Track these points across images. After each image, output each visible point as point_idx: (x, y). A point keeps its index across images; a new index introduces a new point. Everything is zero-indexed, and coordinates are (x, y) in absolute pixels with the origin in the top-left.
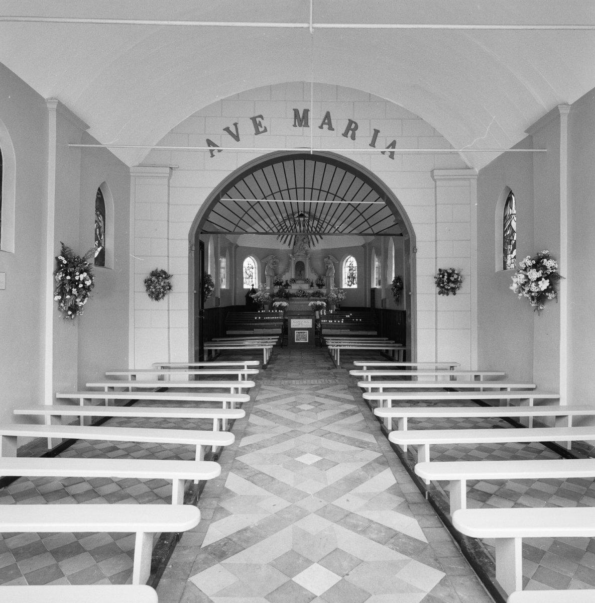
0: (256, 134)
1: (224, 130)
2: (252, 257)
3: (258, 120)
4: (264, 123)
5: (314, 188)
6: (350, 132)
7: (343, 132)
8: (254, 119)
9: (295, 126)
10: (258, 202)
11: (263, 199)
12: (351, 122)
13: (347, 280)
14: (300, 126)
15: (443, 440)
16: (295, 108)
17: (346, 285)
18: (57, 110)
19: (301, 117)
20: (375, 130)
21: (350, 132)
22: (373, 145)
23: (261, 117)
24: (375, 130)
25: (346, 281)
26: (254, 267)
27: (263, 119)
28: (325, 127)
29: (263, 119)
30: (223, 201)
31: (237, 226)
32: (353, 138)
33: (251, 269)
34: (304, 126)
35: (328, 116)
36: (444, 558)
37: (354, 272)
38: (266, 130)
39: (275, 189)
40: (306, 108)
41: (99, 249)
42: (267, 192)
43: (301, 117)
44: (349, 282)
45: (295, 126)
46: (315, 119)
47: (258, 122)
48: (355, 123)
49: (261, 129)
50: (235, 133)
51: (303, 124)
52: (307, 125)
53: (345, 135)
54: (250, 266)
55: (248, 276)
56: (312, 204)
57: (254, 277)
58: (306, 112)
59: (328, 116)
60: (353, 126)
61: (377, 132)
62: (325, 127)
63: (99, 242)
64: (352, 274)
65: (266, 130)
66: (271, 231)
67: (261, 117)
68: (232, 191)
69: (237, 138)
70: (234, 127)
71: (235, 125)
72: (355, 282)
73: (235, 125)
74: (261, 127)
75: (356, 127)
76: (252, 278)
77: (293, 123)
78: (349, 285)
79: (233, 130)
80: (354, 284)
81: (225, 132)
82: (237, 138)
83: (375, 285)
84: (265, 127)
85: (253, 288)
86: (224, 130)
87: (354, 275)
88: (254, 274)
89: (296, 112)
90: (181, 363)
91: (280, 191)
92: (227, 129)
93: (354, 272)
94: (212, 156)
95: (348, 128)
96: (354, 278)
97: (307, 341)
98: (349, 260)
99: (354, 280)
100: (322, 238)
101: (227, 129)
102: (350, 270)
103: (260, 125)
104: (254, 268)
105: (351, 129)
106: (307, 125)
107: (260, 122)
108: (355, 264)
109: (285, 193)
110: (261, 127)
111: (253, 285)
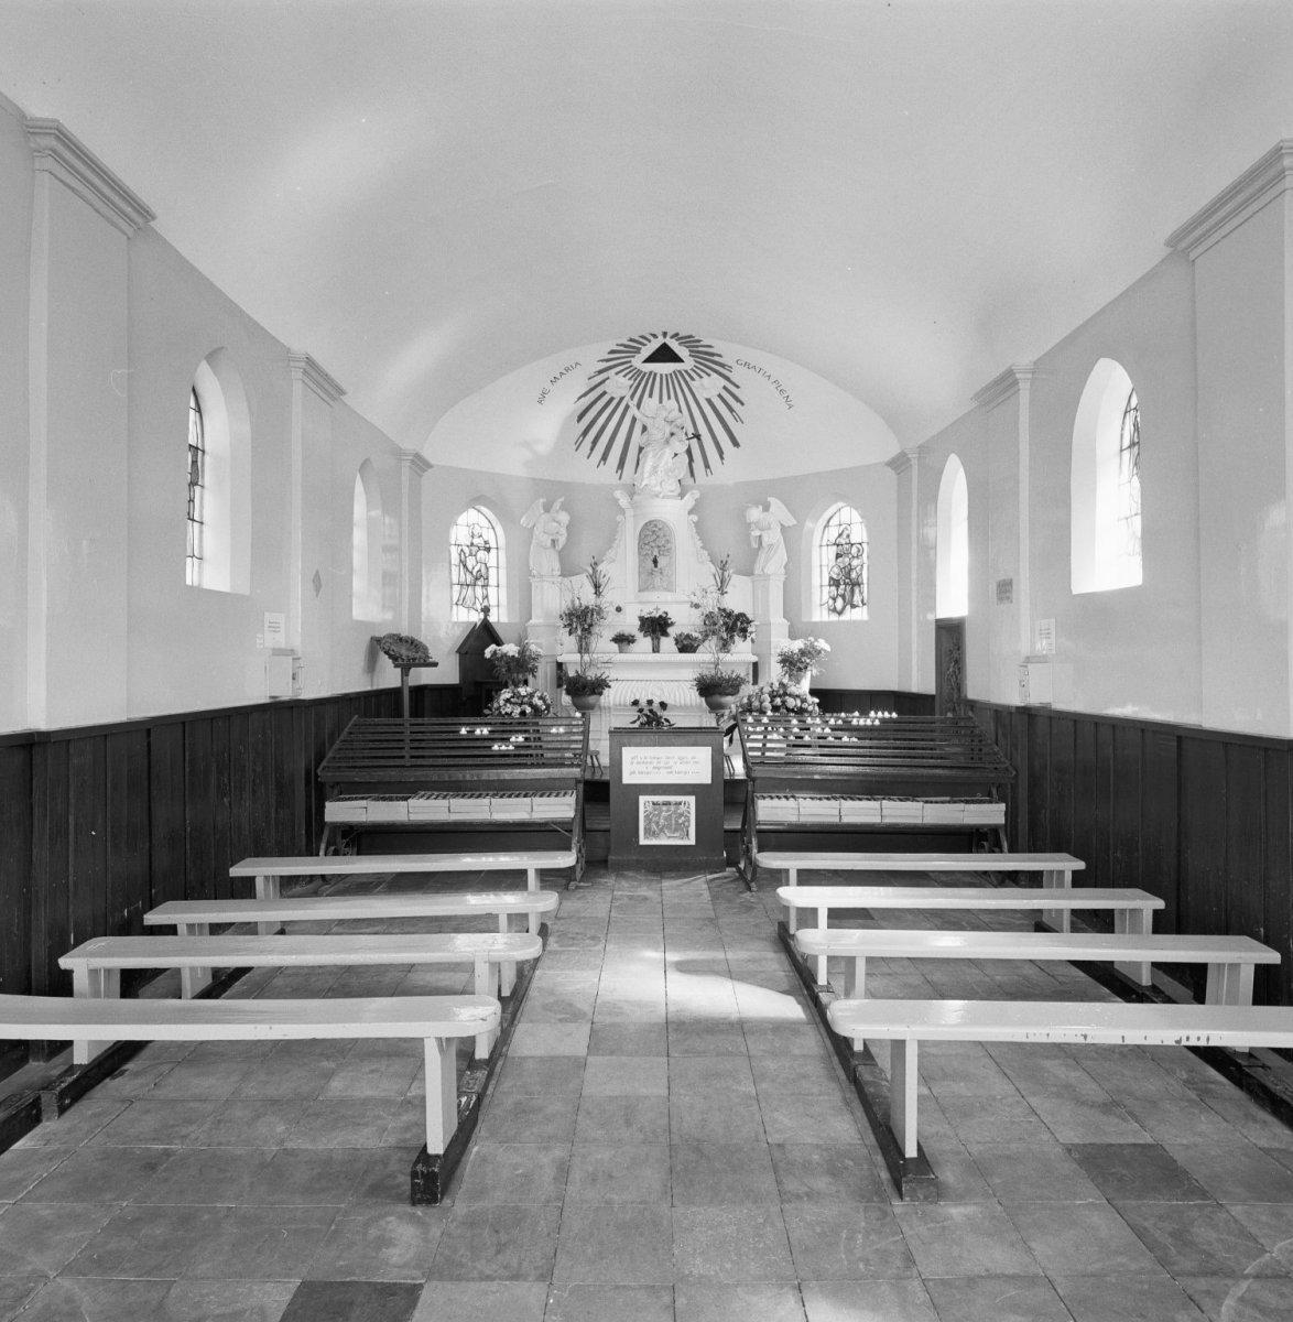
2: (483, 509)
13: (828, 591)
17: (825, 612)
25: (826, 597)
26: (493, 544)
33: (482, 554)
37: (855, 562)
44: (834, 599)
54: (476, 541)
55: (469, 579)
64: (848, 570)
72: (857, 599)
76: (485, 586)
78: (834, 610)
80: (853, 606)
83: (953, 602)
87: (854, 575)
88: (492, 573)
90: (942, 802)
93: (855, 562)
97: (643, 841)
98: (834, 521)
99: (852, 592)
100: (736, 443)
102: (838, 556)
108: (859, 534)
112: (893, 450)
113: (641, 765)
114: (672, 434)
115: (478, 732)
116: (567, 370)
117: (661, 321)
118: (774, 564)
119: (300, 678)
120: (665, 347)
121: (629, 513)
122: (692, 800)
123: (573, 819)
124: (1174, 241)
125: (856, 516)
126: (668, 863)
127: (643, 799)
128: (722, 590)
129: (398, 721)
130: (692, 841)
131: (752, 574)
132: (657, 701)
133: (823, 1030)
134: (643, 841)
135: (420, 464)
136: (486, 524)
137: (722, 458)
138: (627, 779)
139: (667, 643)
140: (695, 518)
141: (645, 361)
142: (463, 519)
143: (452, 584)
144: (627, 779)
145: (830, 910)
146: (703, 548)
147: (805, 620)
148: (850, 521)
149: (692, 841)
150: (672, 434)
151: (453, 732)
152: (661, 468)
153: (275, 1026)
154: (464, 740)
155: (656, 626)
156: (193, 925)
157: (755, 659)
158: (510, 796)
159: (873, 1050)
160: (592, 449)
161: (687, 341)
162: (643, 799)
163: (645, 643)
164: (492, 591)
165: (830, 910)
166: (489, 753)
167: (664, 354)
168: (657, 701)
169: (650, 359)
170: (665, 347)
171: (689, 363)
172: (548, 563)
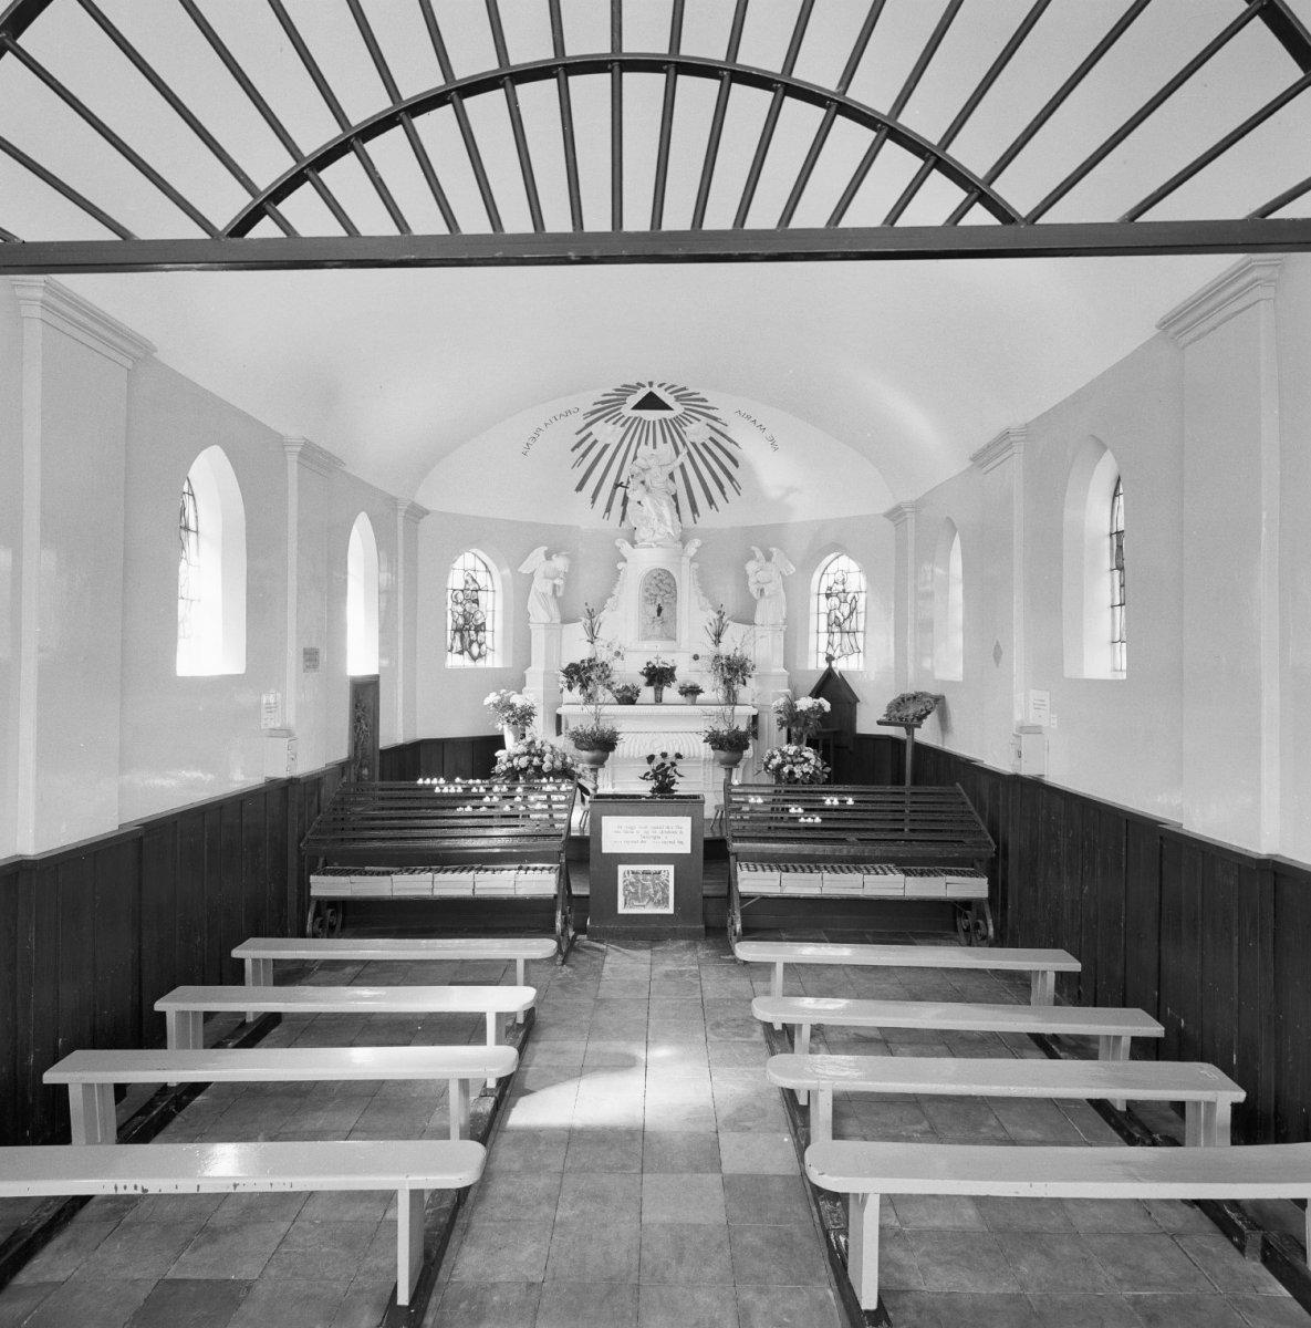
26: (823, 598)
88: (823, 627)
96: (459, 630)
97: (621, 910)
108: (856, 581)
112: (888, 505)
113: (619, 835)
114: (643, 482)
115: (836, 802)
116: (749, 417)
117: (654, 372)
118: (768, 612)
119: (1013, 751)
120: (651, 395)
122: (671, 868)
123: (556, 897)
124: (1165, 324)
125: (853, 566)
126: (645, 932)
127: (622, 869)
128: (717, 642)
129: (900, 789)
130: (670, 910)
131: (751, 622)
132: (671, 754)
133: (499, 1114)
134: (621, 910)
135: (417, 513)
136: (483, 568)
137: (593, 502)
138: (606, 849)
139: (671, 693)
140: (696, 565)
141: (633, 408)
142: (459, 564)
143: (864, 632)
144: (606, 849)
145: (785, 964)
146: (612, 596)
147: (800, 668)
148: (844, 570)
149: (670, 910)
150: (643, 482)
151: (817, 801)
152: (654, 515)
153: (1050, 1184)
154: (850, 810)
155: (659, 676)
156: (91, 1085)
157: (755, 712)
158: (454, 871)
159: (1136, 1111)
160: (724, 493)
161: (683, 395)
162: (622, 869)
163: (648, 693)
164: (823, 647)
165: (785, 964)
166: (795, 825)
167: (651, 402)
168: (671, 754)
169: (638, 407)
170: (651, 395)
171: (678, 409)
172: (541, 613)
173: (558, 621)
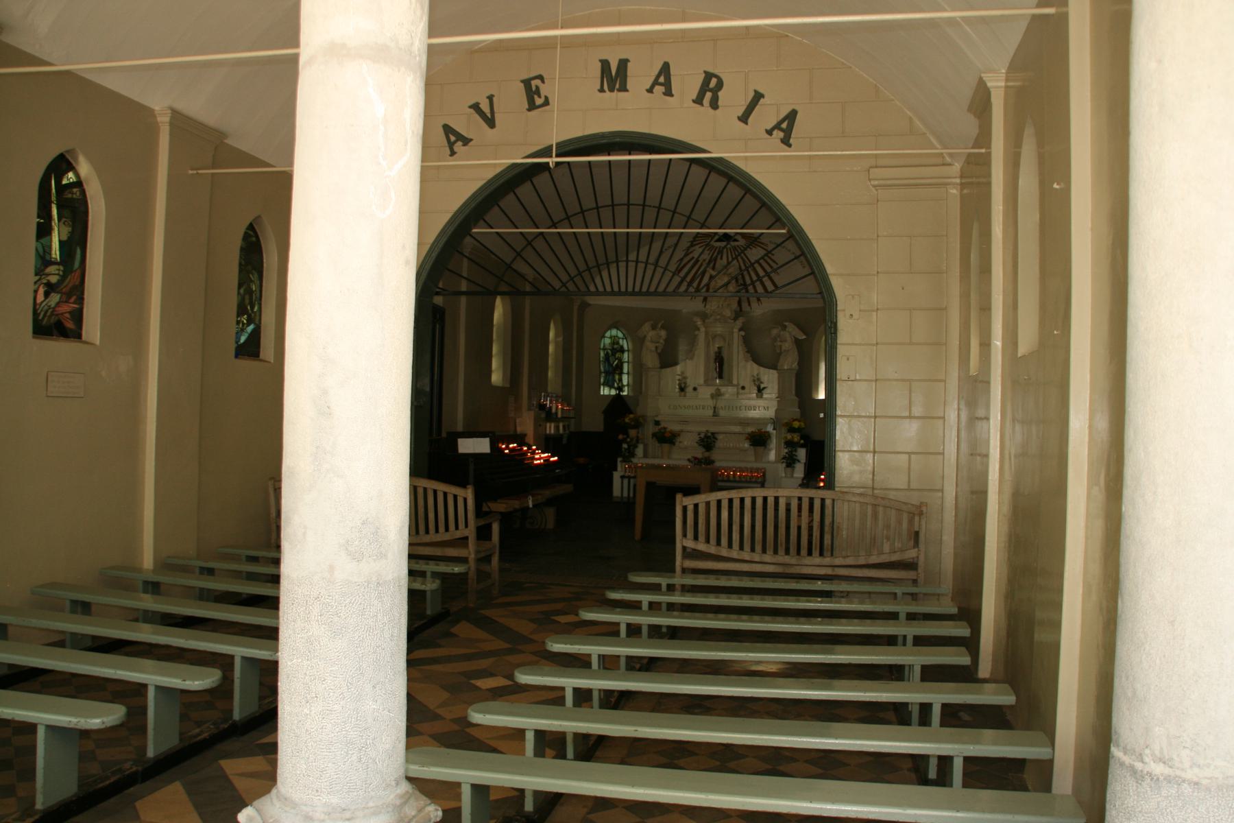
0: (529, 110)
1: (470, 107)
3: (534, 83)
4: (545, 90)
5: (565, 216)
6: (709, 95)
7: (769, 127)
8: (527, 83)
9: (602, 90)
10: (542, 234)
11: (549, 228)
12: (708, 76)
14: (612, 90)
15: (885, 658)
16: (604, 58)
18: (171, 124)
19: (614, 72)
20: (755, 91)
21: (709, 95)
22: (744, 118)
23: (541, 78)
24: (755, 91)
26: (625, 347)
27: (543, 82)
28: (458, 146)
29: (543, 82)
30: (476, 233)
31: (674, 212)
32: (714, 105)
34: (619, 90)
35: (665, 69)
36: (859, 416)
38: (546, 103)
39: (588, 203)
40: (624, 57)
41: (251, 327)
42: (558, 214)
43: (614, 72)
45: (602, 90)
46: (640, 77)
47: (534, 89)
48: (716, 76)
49: (539, 101)
50: (489, 115)
51: (617, 86)
52: (624, 88)
53: (699, 101)
54: (616, 346)
56: (653, 225)
57: (625, 370)
58: (623, 64)
59: (665, 69)
60: (714, 82)
61: (758, 96)
62: (659, 89)
63: (249, 316)
65: (546, 103)
66: (563, 289)
67: (541, 78)
68: (494, 214)
69: (491, 123)
70: (487, 101)
71: (490, 98)
73: (490, 98)
74: (540, 97)
75: (720, 84)
77: (599, 87)
79: (485, 107)
81: (472, 111)
82: (491, 123)
84: (546, 98)
85: (618, 397)
86: (470, 107)
88: (625, 366)
89: (605, 64)
91: (613, 205)
92: (476, 107)
94: (650, 91)
95: (704, 88)
101: (476, 107)
103: (538, 92)
104: (626, 355)
105: (710, 89)
106: (624, 88)
107: (537, 87)
109: (592, 216)
110: (540, 97)
111: (620, 389)
121: (703, 329)
142: (608, 334)
173: (657, 364)
